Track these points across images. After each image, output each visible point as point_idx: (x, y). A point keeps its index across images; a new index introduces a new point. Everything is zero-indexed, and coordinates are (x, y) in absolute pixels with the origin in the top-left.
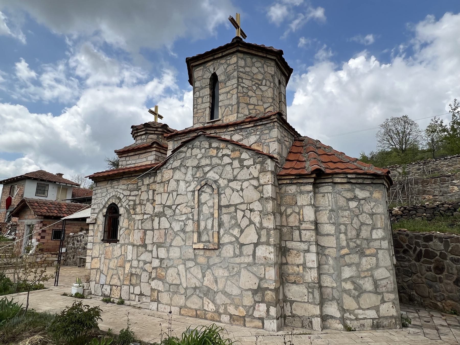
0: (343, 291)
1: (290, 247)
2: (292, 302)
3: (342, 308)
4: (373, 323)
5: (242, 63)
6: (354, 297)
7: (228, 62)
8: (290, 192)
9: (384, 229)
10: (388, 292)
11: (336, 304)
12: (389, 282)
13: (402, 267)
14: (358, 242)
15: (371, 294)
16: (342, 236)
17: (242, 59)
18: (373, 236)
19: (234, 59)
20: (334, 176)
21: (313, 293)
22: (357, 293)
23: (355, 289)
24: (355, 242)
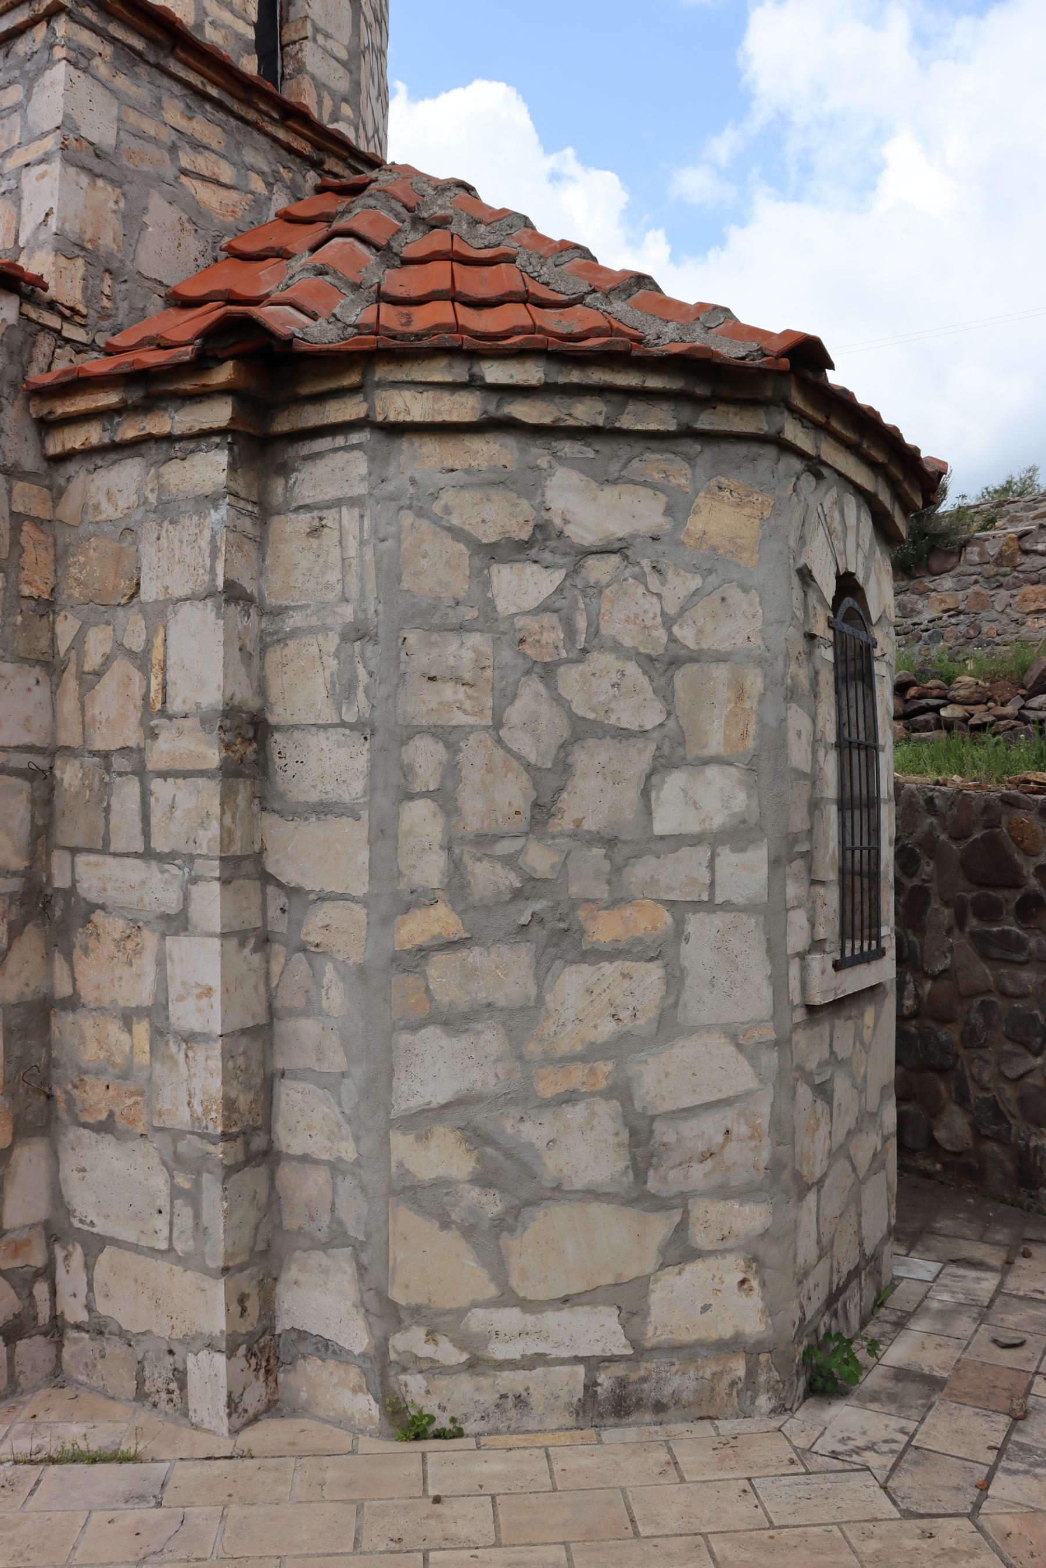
0: (391, 1192)
1: (93, 897)
2: (95, 1245)
3: (381, 1295)
4: (590, 1386)
6: (468, 1232)
8: (108, 511)
9: (752, 769)
10: (723, 1192)
11: (349, 1269)
12: (741, 1129)
13: (1004, 994)
14: (540, 859)
15: (598, 1210)
16: (420, 819)
18: (658, 812)
20: (383, 372)
21: (193, 1197)
22: (493, 1205)
23: (484, 1180)
24: (510, 861)
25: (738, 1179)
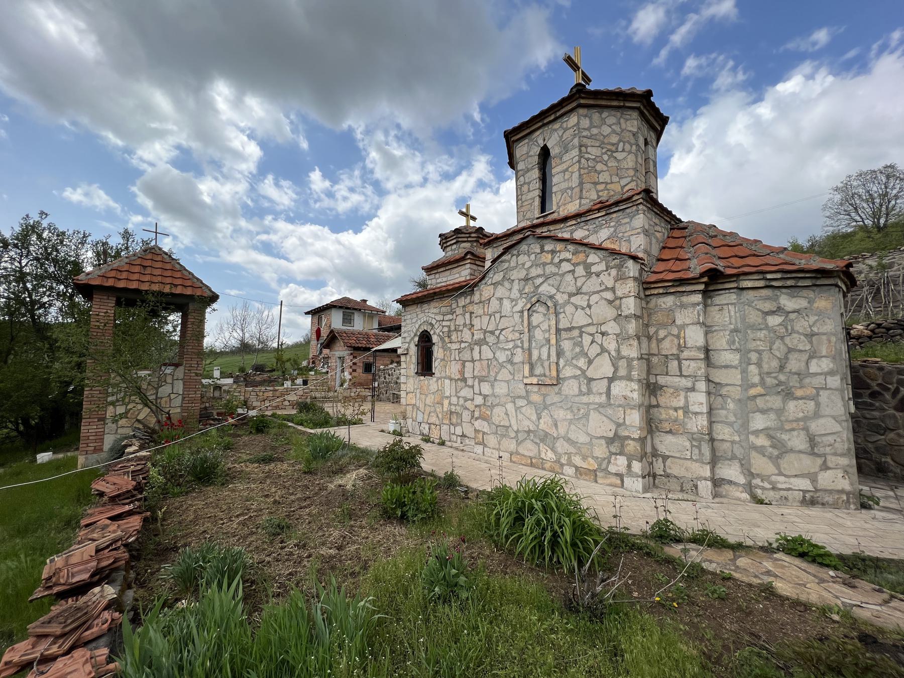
0: (750, 448)
2: (665, 458)
4: (804, 497)
5: (585, 123)
6: (770, 458)
7: (565, 125)
9: (834, 358)
10: (835, 454)
11: (738, 465)
12: (838, 440)
14: (782, 378)
15: (802, 456)
16: (753, 369)
17: (586, 116)
19: (573, 120)
22: (776, 453)
24: (775, 378)
25: (839, 452)
